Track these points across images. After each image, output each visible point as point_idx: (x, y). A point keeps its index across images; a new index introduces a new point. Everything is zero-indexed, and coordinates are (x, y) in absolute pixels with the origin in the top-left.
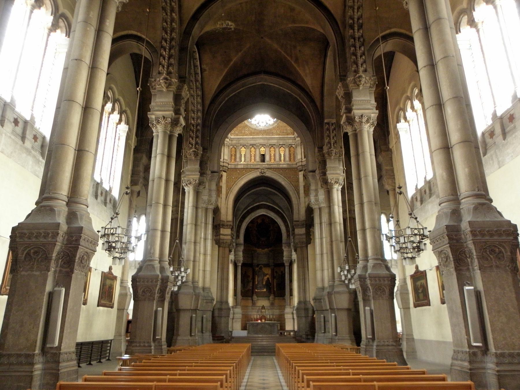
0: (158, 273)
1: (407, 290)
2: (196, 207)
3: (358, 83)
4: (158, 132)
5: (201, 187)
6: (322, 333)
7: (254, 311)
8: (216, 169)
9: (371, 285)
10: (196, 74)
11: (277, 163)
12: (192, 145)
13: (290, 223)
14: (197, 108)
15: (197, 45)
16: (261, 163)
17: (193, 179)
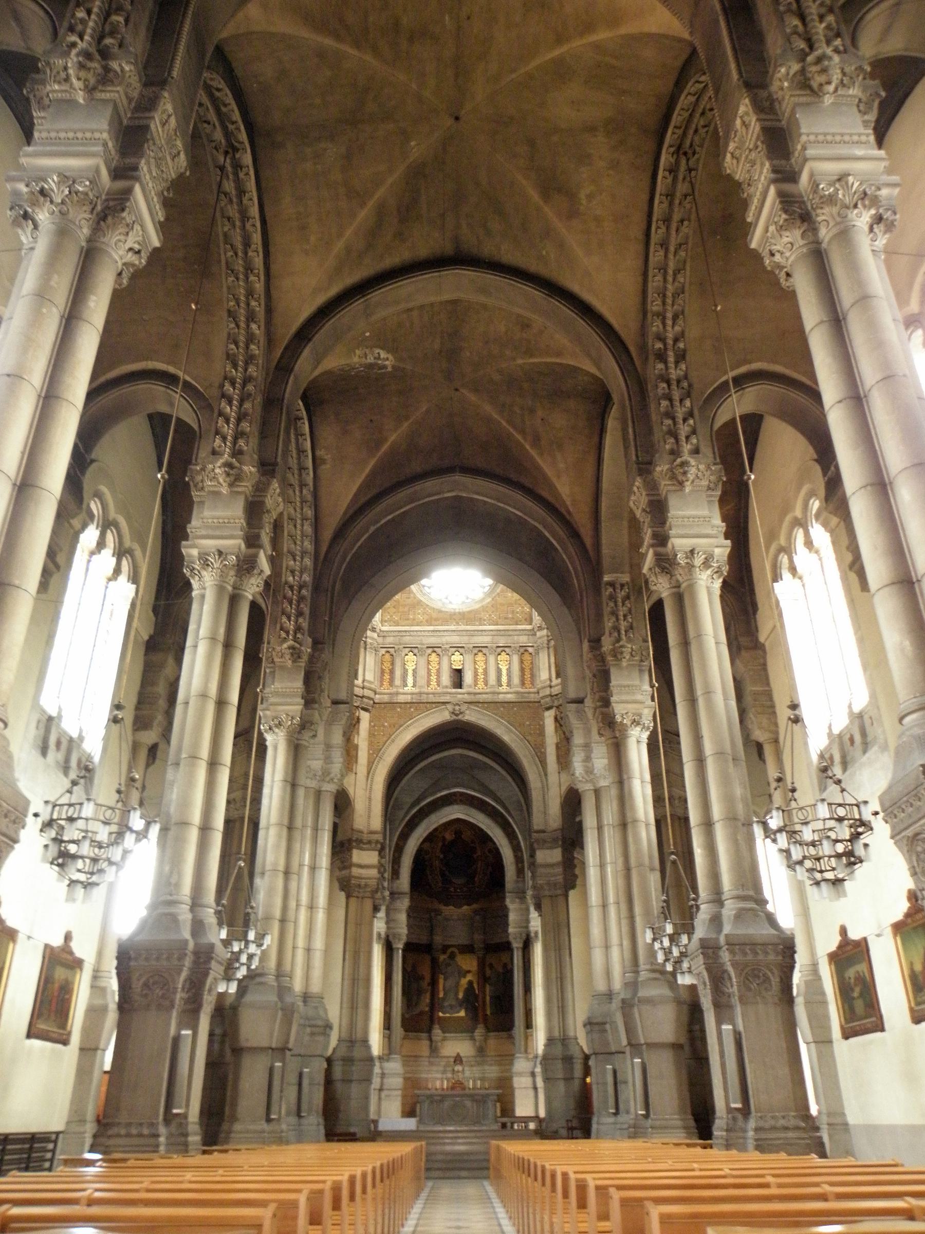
0: (186, 934)
1: (823, 994)
2: (292, 784)
3: (680, 478)
4: (204, 588)
5: (307, 735)
6: (609, 1114)
7: (435, 1068)
8: (343, 696)
9: (732, 965)
10: (302, 468)
11: (492, 690)
12: (287, 633)
13: (525, 839)
14: (302, 547)
15: (305, 397)
16: (454, 690)
17: (287, 715)
